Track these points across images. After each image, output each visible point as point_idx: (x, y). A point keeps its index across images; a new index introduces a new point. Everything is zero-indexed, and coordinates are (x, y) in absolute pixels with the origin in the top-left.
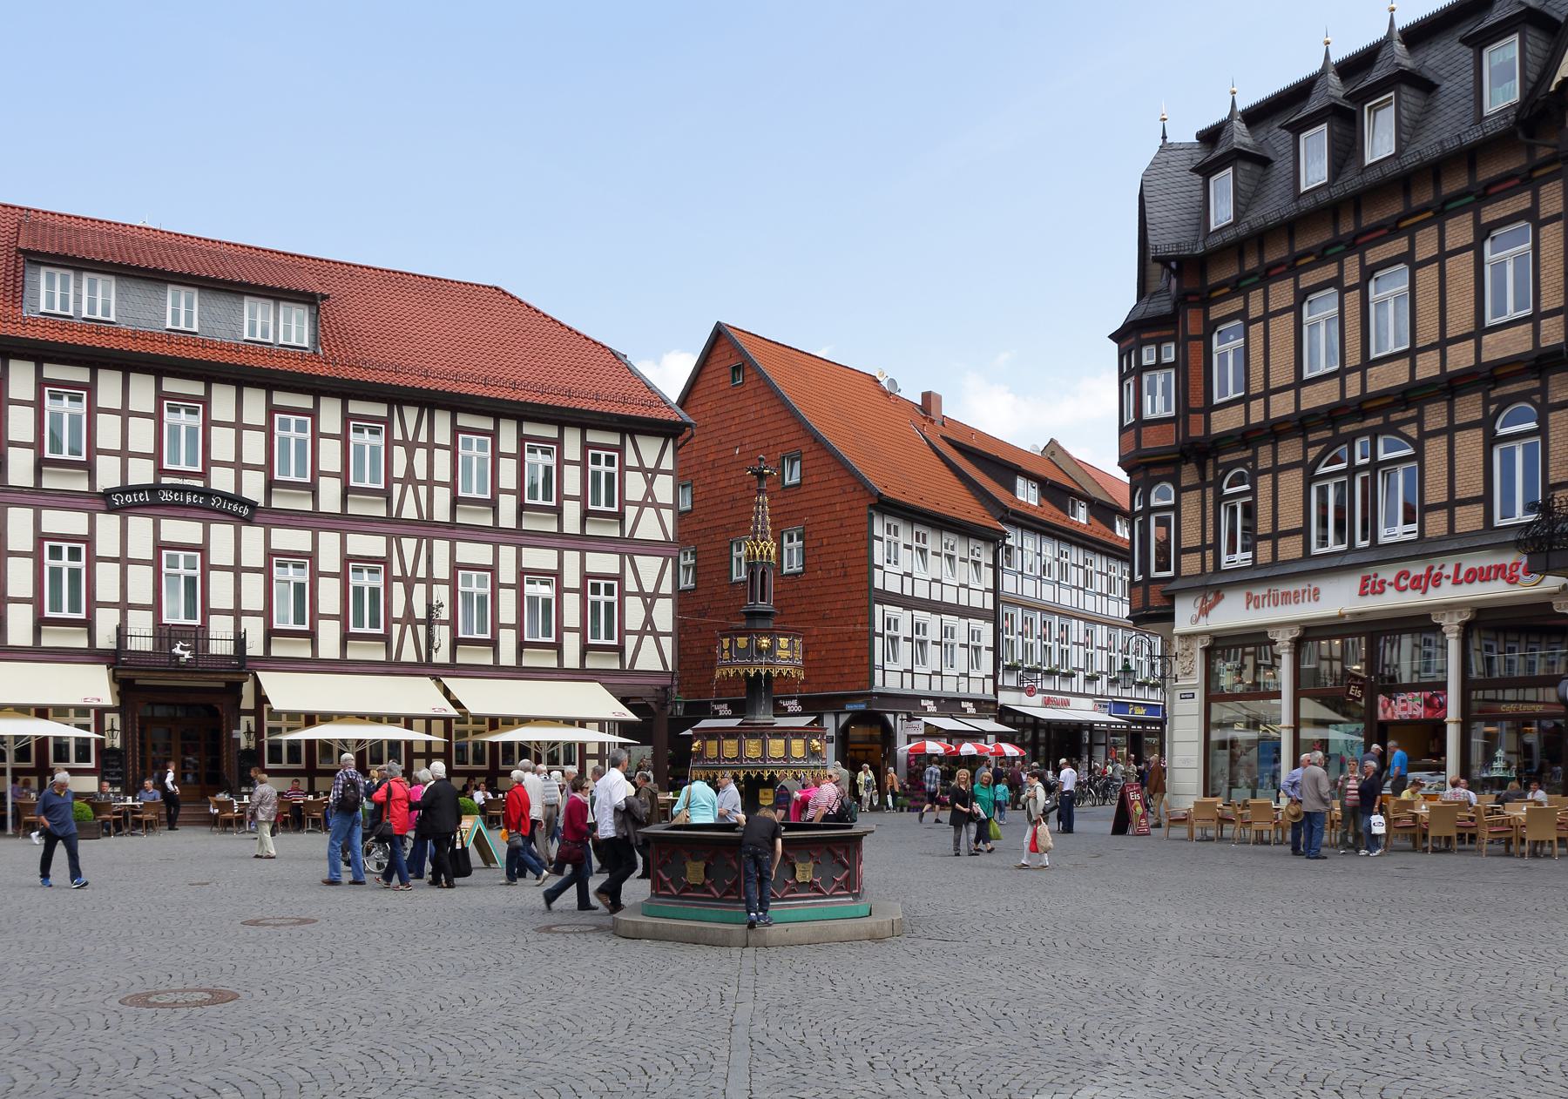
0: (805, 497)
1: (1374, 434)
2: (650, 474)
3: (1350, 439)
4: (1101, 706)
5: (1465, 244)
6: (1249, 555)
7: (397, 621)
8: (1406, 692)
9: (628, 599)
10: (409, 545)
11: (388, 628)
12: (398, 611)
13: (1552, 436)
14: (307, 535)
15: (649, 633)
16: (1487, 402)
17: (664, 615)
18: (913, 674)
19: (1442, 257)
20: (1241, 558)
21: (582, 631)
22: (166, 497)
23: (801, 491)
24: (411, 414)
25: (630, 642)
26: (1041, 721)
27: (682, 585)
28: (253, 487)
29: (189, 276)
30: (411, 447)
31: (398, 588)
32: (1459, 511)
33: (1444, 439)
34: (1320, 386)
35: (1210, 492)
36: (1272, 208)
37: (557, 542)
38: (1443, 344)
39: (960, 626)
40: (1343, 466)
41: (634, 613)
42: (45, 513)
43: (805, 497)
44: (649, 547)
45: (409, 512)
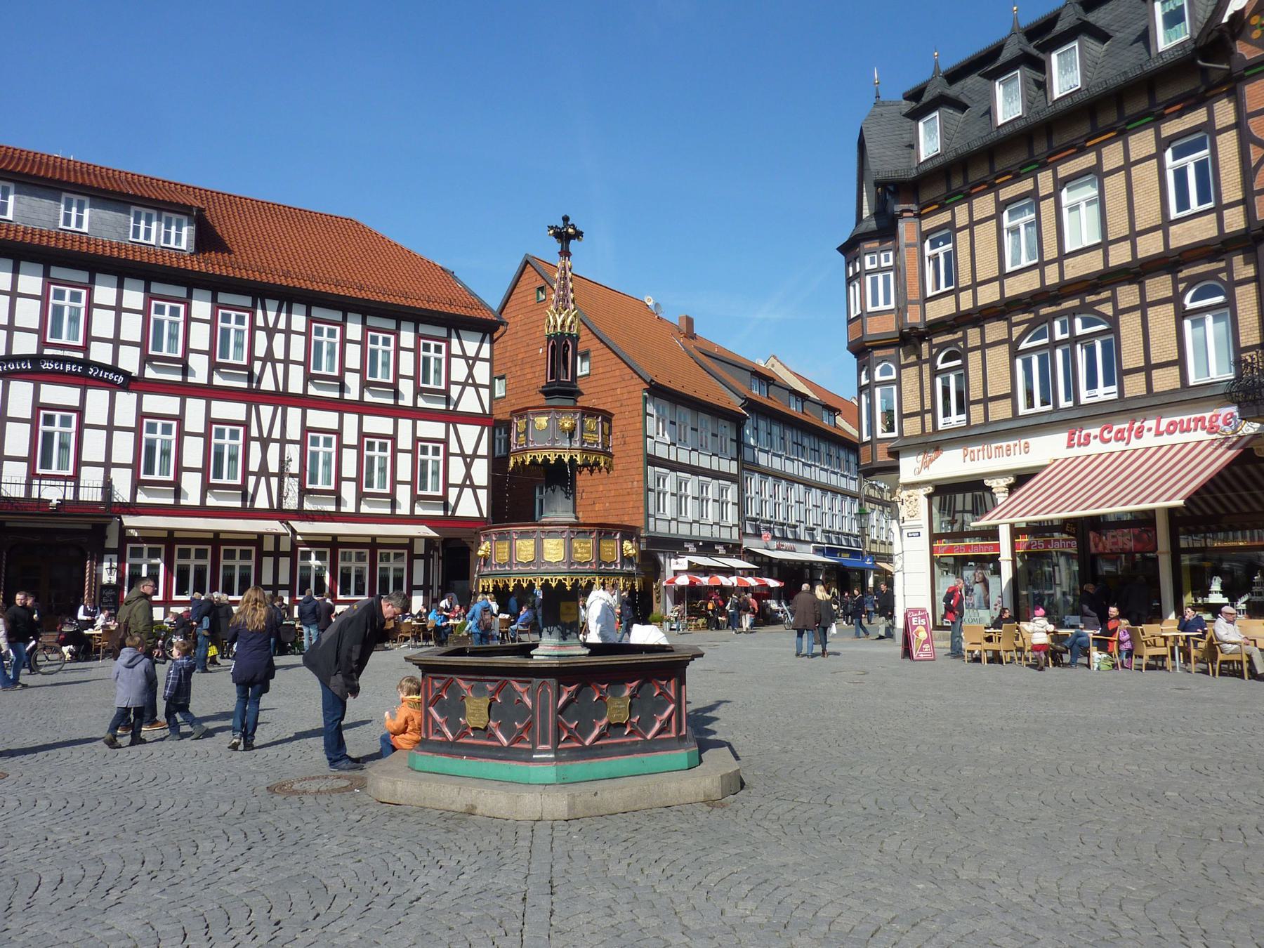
0: (594, 384)
1: (1072, 313)
2: (471, 361)
3: (1051, 318)
4: (817, 551)
5: (1147, 154)
6: (963, 417)
7: (253, 474)
8: (1116, 529)
9: (451, 458)
10: (266, 411)
11: (245, 480)
12: (254, 466)
13: (1240, 307)
14: (176, 401)
15: (468, 486)
16: (1176, 283)
17: (481, 472)
18: (678, 522)
19: (1127, 166)
20: (956, 420)
21: (413, 483)
22: (47, 366)
23: (590, 380)
24: (272, 304)
25: (453, 493)
26: (774, 561)
27: (497, 454)
28: (130, 361)
29: (83, 186)
30: (271, 332)
31: (255, 447)
32: (1155, 373)
33: (1138, 313)
34: (1022, 277)
35: (926, 367)
36: (975, 137)
37: (82, 380)
38: (1133, 236)
39: (713, 487)
40: (1046, 341)
41: (457, 471)
42: (366, 418)
43: (594, 384)
44: (469, 418)
45: (268, 384)
